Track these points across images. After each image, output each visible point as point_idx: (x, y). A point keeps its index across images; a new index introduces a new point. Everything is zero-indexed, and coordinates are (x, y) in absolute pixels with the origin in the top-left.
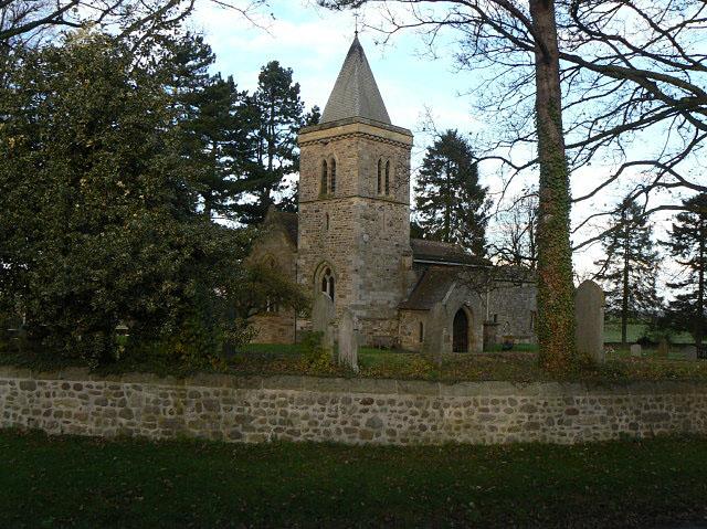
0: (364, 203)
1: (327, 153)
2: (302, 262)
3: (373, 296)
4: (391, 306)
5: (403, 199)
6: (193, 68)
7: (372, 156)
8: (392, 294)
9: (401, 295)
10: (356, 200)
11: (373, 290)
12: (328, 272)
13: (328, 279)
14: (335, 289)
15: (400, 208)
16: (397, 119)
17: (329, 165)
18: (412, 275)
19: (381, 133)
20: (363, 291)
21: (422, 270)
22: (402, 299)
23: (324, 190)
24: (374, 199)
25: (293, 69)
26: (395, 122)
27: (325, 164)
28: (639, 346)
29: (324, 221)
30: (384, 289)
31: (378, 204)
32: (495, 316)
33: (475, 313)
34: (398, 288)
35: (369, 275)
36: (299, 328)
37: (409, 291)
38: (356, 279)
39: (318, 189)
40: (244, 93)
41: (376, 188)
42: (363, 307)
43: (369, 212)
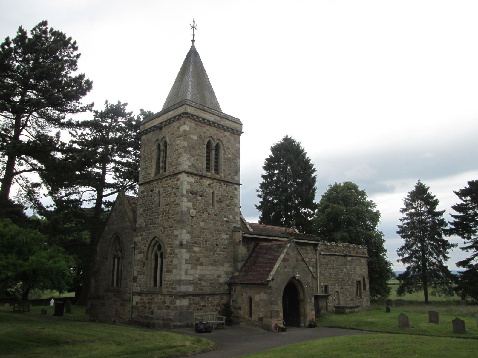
0: (191, 179)
1: (160, 137)
2: (138, 239)
3: (200, 270)
4: (221, 280)
5: (233, 179)
6: (415, 243)
7: (200, 137)
8: (221, 268)
9: (230, 269)
10: (183, 177)
11: (202, 264)
12: (160, 247)
13: (159, 254)
14: (164, 264)
15: (230, 188)
16: (227, 108)
17: (162, 148)
18: (242, 250)
19: (211, 118)
20: (189, 266)
21: (252, 244)
22: (233, 273)
23: (157, 172)
24: (202, 176)
25: (79, 48)
26: (223, 112)
27: (159, 146)
28: (296, 260)
29: (156, 199)
30: (214, 263)
31: (206, 182)
32: (326, 286)
33: (305, 287)
34: (229, 262)
35: (196, 249)
36: (134, 304)
37: (240, 265)
38: (185, 255)
39: (154, 170)
40: (130, 114)
41: (205, 166)
42: (190, 283)
43: (197, 188)
